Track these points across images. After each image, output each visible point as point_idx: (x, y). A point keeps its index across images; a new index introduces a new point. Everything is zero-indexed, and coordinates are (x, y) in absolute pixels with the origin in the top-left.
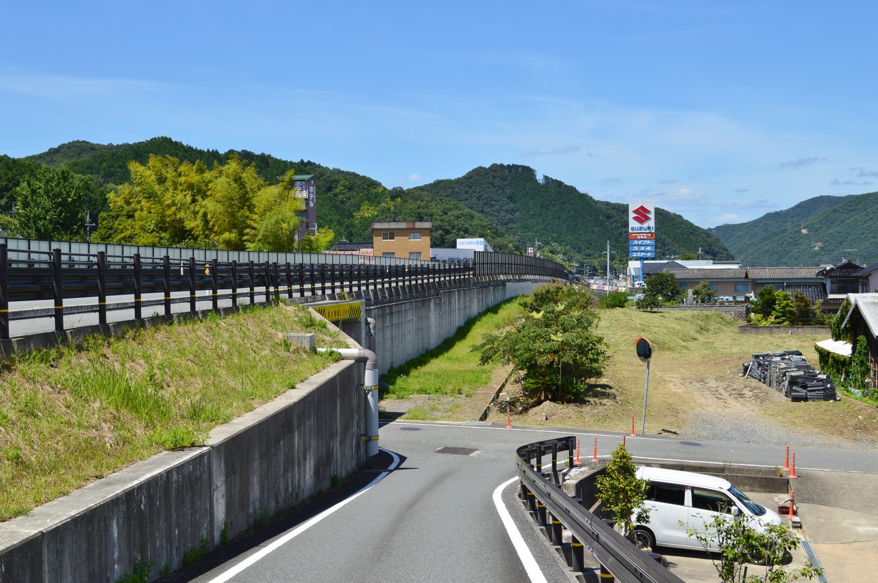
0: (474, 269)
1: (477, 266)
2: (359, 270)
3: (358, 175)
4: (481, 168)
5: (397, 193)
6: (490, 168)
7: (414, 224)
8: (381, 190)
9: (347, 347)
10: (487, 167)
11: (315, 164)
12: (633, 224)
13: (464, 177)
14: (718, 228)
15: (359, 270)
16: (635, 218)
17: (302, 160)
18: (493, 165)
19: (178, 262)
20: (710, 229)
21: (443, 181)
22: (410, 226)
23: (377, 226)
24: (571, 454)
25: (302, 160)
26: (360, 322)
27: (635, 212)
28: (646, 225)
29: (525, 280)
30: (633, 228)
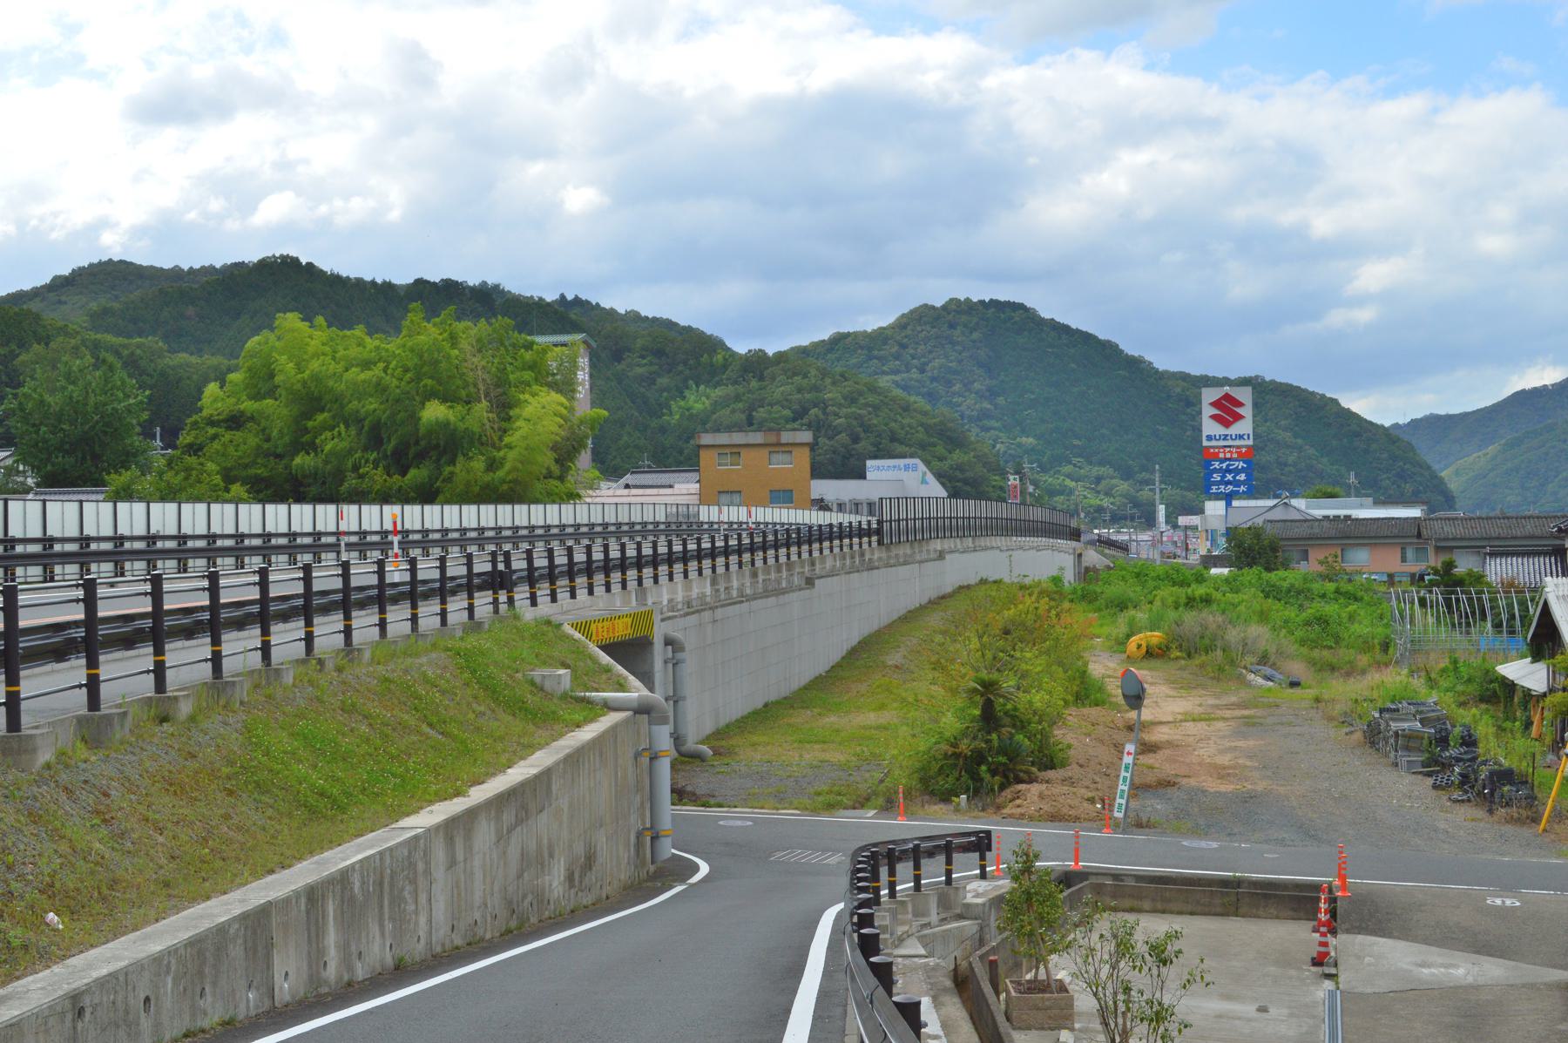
0: (879, 532)
1: (886, 526)
2: (804, 530)
3: (676, 324)
4: (926, 305)
5: (757, 364)
6: (944, 307)
7: (779, 436)
8: (719, 358)
9: (621, 687)
10: (938, 304)
11: (588, 302)
12: (1210, 428)
13: (892, 327)
14: (1415, 424)
15: (804, 530)
16: (1214, 417)
17: (563, 296)
18: (951, 300)
19: (331, 540)
20: (1396, 426)
21: (849, 334)
22: (772, 439)
23: (706, 439)
24: (983, 858)
25: (563, 296)
26: (651, 644)
27: (1215, 404)
28: (1237, 429)
29: (986, 549)
30: (1209, 438)
